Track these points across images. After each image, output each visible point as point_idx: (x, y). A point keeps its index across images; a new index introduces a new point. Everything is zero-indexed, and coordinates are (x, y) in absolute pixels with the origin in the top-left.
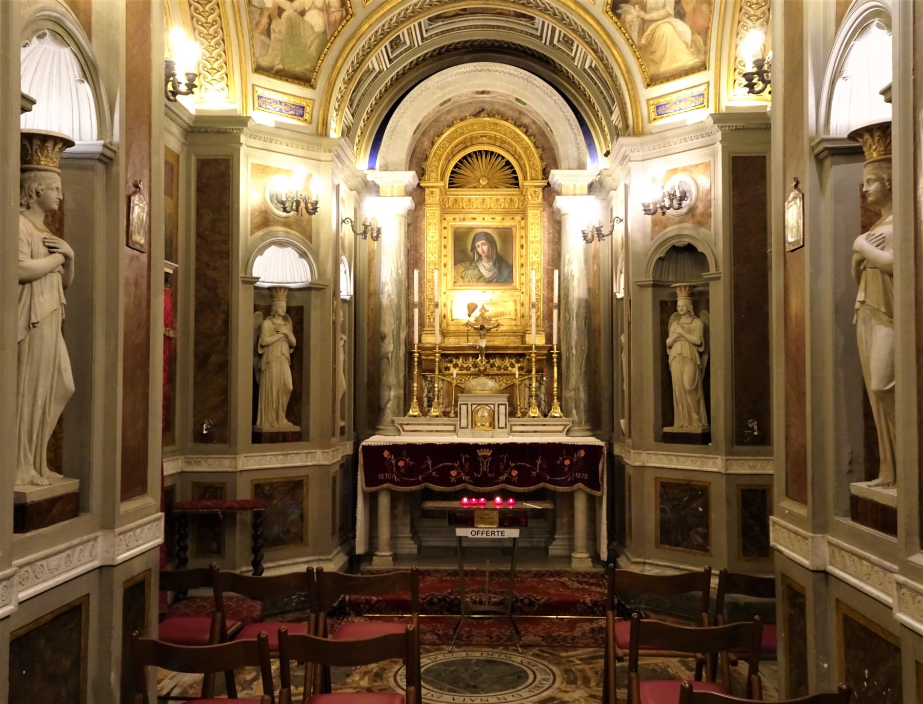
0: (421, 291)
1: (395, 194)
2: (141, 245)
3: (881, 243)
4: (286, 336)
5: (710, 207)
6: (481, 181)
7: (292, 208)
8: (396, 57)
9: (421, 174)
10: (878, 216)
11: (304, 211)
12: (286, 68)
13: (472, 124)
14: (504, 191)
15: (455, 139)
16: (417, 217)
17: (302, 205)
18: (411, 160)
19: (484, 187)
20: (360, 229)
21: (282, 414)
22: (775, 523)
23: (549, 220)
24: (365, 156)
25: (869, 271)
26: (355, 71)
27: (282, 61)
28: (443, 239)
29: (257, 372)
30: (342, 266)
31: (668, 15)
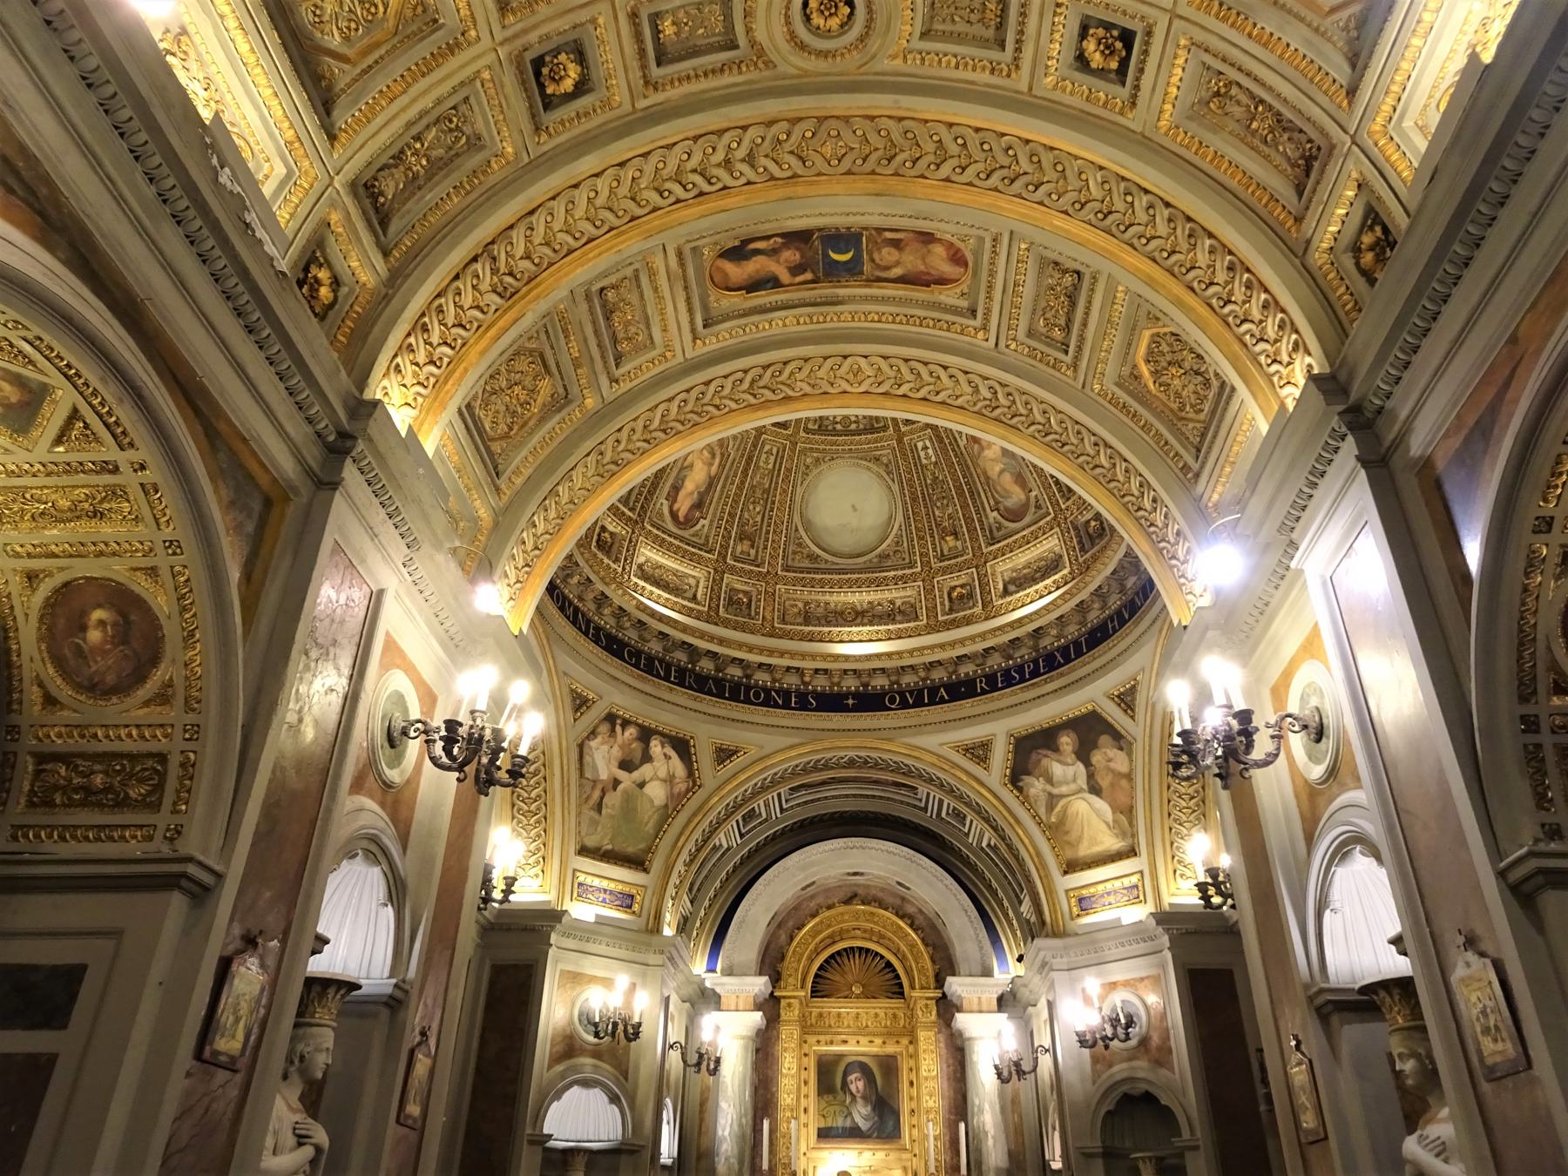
0: (772, 1152)
1: (741, 1008)
2: (415, 1120)
5: (1169, 1039)
7: (606, 1032)
8: (749, 831)
9: (776, 979)
10: (1426, 1107)
11: (622, 1035)
12: (616, 849)
13: (842, 914)
15: (821, 932)
16: (769, 1039)
17: (621, 1027)
18: (763, 961)
19: (858, 997)
20: (693, 1059)
23: (947, 1045)
24: (703, 954)
26: (698, 850)
27: (612, 841)
28: (803, 1072)
30: (665, 1113)
31: (1080, 790)
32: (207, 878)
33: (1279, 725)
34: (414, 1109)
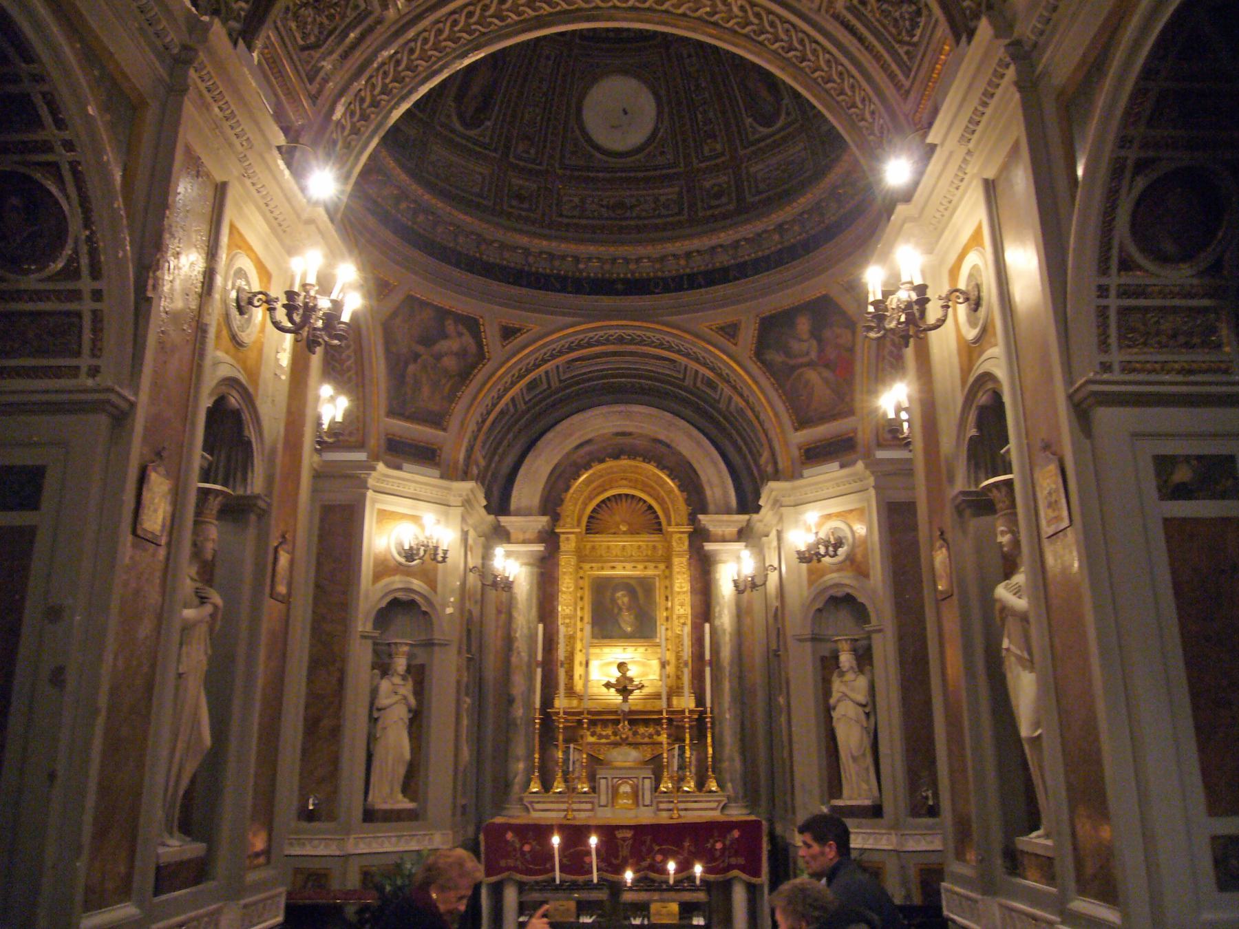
2: (283, 596)
3: (1017, 592)
4: (405, 698)
6: (621, 527)
14: (645, 537)
19: (624, 533)
21: (398, 788)
22: (947, 890)
25: (1010, 617)
32: (124, 405)
33: (948, 298)
34: (282, 589)
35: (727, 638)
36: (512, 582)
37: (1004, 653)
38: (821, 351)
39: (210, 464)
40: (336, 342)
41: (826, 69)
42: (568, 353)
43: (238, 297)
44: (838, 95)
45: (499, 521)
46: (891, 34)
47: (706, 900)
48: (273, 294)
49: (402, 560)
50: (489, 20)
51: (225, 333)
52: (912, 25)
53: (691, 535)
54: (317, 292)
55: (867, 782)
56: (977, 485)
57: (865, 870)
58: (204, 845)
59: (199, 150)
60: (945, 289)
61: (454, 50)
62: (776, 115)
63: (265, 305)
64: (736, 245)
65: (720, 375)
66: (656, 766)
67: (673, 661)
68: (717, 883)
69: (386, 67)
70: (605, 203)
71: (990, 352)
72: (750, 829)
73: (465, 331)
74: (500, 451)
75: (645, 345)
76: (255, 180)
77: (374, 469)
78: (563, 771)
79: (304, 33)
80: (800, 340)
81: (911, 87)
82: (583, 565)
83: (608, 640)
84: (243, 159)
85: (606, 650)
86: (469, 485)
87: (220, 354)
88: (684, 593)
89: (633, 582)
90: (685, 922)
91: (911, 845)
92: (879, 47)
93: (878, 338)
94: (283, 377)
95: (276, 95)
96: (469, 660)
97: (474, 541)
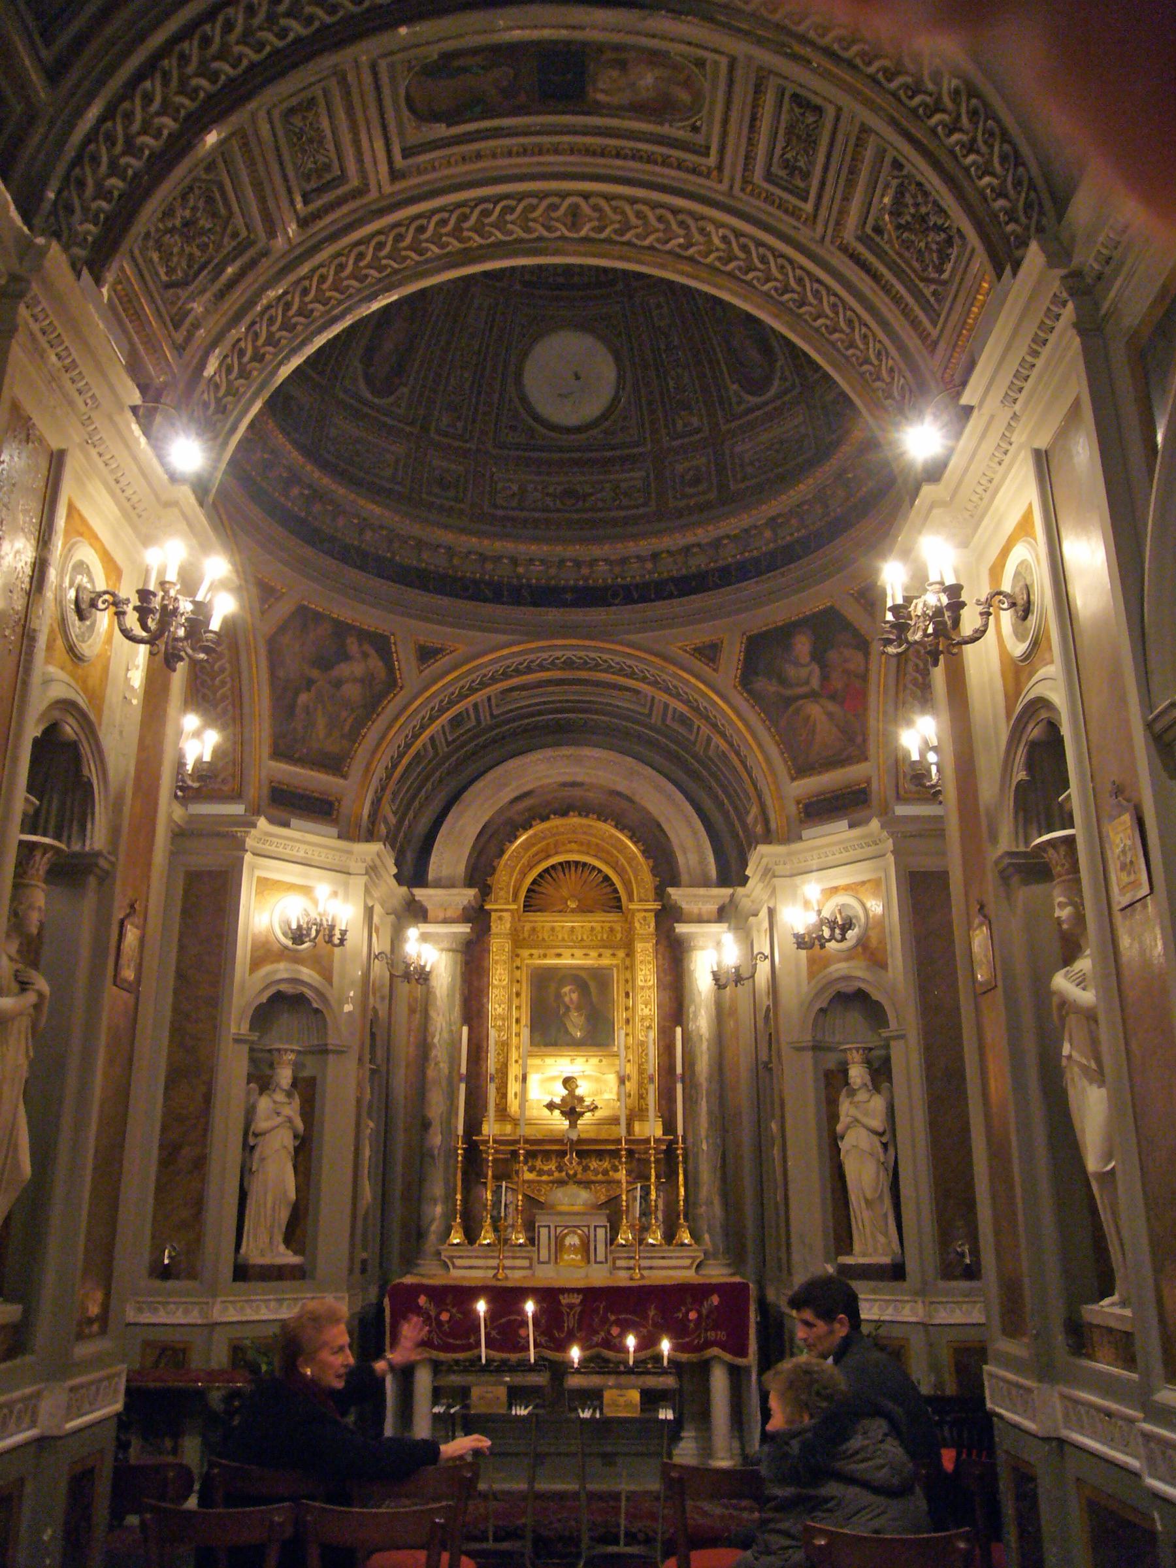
2: (130, 983)
3: (1081, 982)
4: (290, 1120)
14: (599, 916)
19: (573, 911)
21: (279, 1238)
25: (1072, 1016)
28: (515, 984)
29: (245, 1172)
33: (989, 603)
34: (129, 974)
35: (705, 1046)
36: (430, 972)
37: (1064, 1062)
38: (825, 678)
39: (37, 812)
40: (202, 656)
41: (831, 315)
42: (501, 680)
43: (77, 597)
44: (847, 349)
45: (413, 895)
46: (914, 271)
47: (676, 1386)
48: (122, 595)
49: (289, 943)
50: (404, 253)
51: (60, 643)
52: (940, 258)
53: (658, 914)
54: (178, 592)
55: (885, 1234)
56: (1027, 843)
57: (882, 1349)
58: (20, 1307)
59: (29, 407)
60: (984, 592)
61: (359, 291)
62: (767, 381)
63: (112, 609)
64: (716, 544)
65: (696, 709)
66: (612, 1211)
67: (635, 1076)
68: (690, 1364)
69: (273, 311)
70: (551, 490)
71: (1042, 672)
72: (733, 1295)
73: (372, 652)
74: (416, 804)
75: (601, 671)
76: (101, 449)
77: (254, 826)
78: (492, 1217)
79: (167, 266)
80: (797, 664)
81: (939, 337)
82: (520, 951)
83: (551, 1049)
84: (87, 421)
85: (549, 1061)
86: (375, 847)
87: (52, 669)
88: (649, 988)
89: (583, 974)
90: (647, 1415)
91: (943, 1316)
92: (899, 287)
93: (898, 655)
94: (135, 702)
95: (125, 331)
96: (373, 1072)
97: (381, 919)
